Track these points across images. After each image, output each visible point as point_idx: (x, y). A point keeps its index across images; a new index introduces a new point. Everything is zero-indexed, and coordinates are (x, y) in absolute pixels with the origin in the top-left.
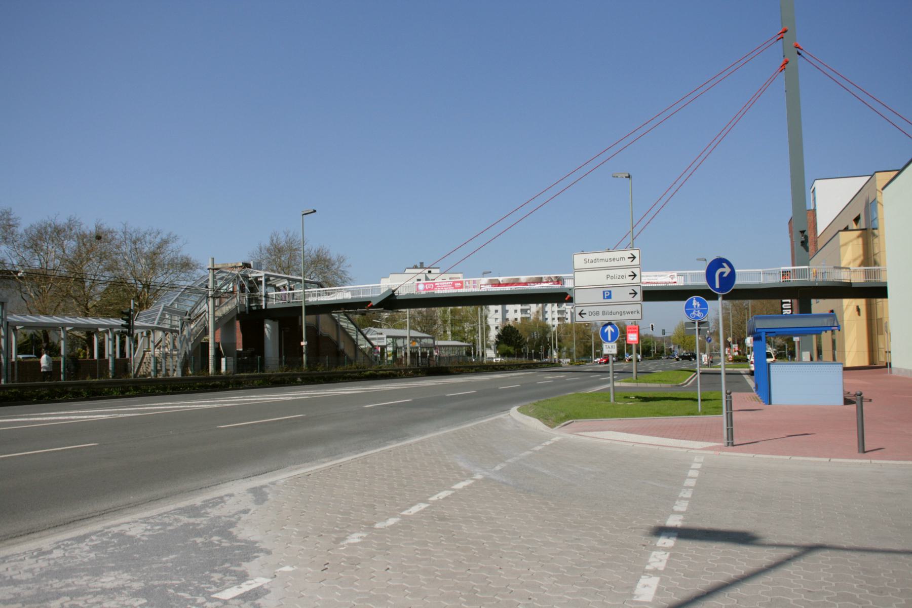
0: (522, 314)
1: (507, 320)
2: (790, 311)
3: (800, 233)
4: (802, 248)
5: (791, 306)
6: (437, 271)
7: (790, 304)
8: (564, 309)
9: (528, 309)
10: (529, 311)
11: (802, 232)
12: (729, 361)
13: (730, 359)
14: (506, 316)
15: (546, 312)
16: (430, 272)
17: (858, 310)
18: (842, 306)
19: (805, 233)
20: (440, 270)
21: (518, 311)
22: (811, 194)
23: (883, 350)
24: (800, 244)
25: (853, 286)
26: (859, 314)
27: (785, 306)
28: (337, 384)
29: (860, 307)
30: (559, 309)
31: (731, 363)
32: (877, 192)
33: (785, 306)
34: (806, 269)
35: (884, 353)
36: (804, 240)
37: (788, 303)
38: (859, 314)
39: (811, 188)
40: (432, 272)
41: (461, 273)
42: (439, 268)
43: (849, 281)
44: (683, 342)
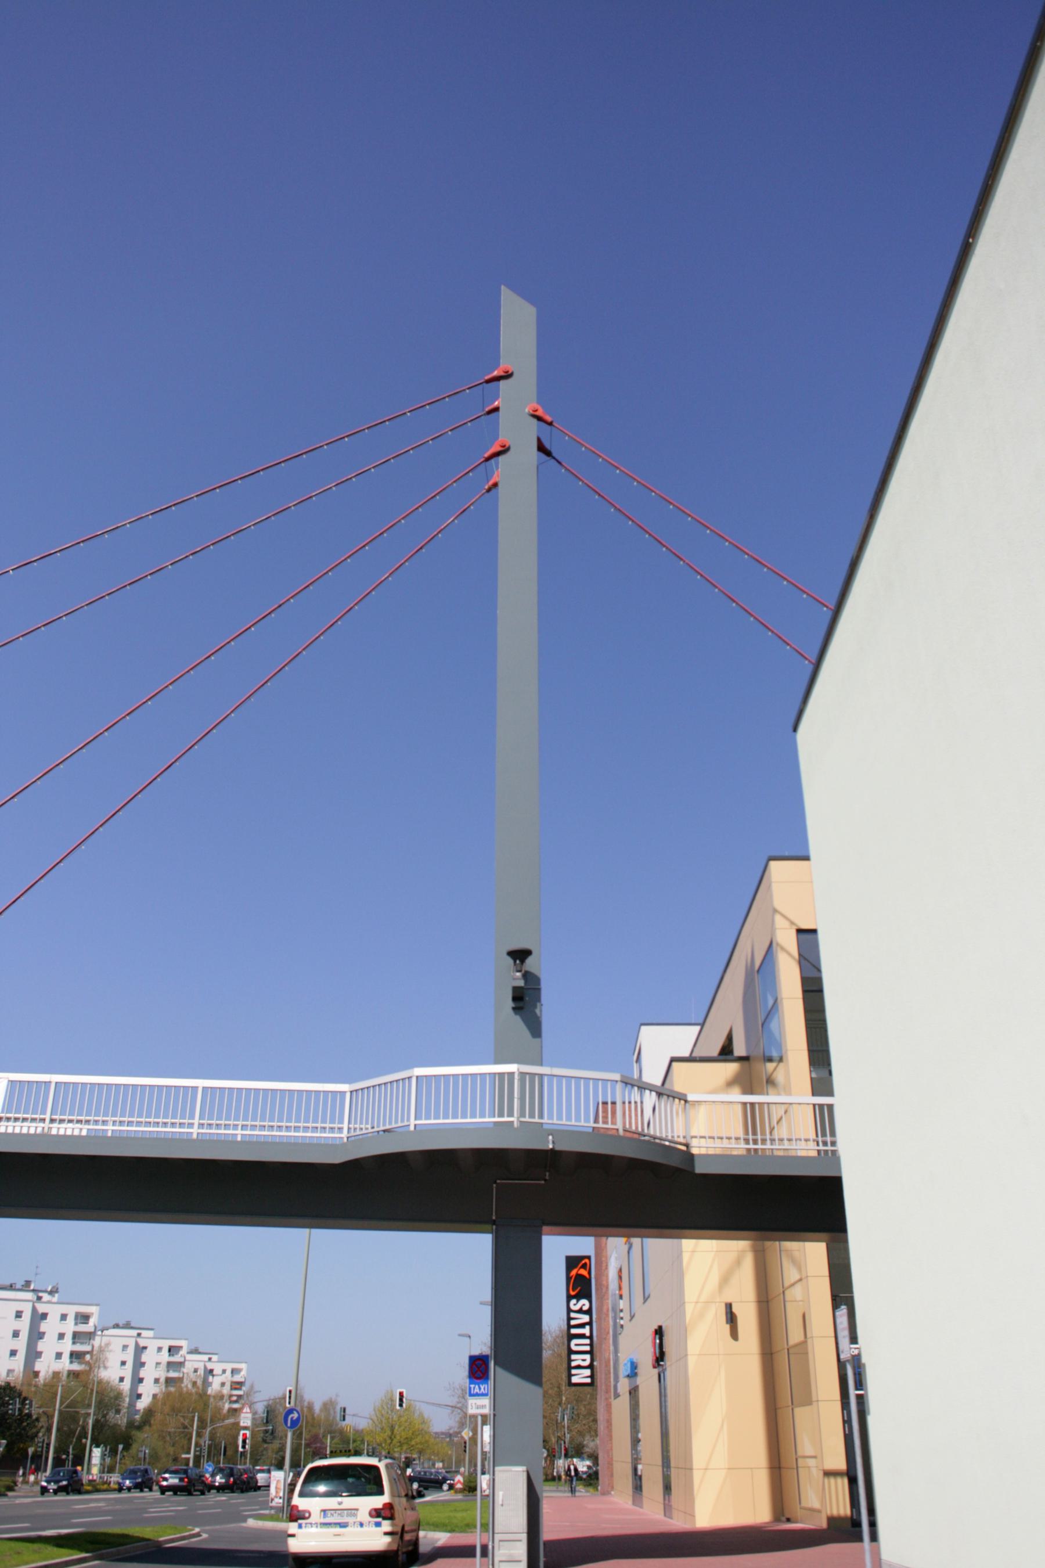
0: (71, 1362)
1: (36, 1374)
2: (588, 1357)
3: (510, 961)
4: (517, 1020)
5: (591, 1345)
6: (150, 1333)
7: (587, 1341)
8: (182, 1360)
9: (88, 1352)
10: (88, 1357)
11: (520, 955)
12: (457, 1491)
13: (459, 1486)
14: (33, 1366)
15: (143, 1364)
16: (210, 1359)
17: (731, 1318)
18: (682, 1304)
19: (530, 963)
20: (154, 1333)
21: (63, 1356)
22: (635, 1064)
23: (812, 1462)
24: (510, 1004)
25: (700, 1169)
26: (734, 1334)
27: (576, 1345)
28: (458, 1545)
29: (735, 1309)
30: (172, 1359)
31: (460, 1496)
32: (778, 917)
33: (576, 1345)
34: (511, 1075)
35: (816, 1474)
36: (521, 983)
37: (582, 1336)
38: (734, 1334)
39: (634, 1054)
40: (142, 1335)
41: (97, 1305)
42: (152, 1329)
43: (684, 1148)
44: (389, 1441)
